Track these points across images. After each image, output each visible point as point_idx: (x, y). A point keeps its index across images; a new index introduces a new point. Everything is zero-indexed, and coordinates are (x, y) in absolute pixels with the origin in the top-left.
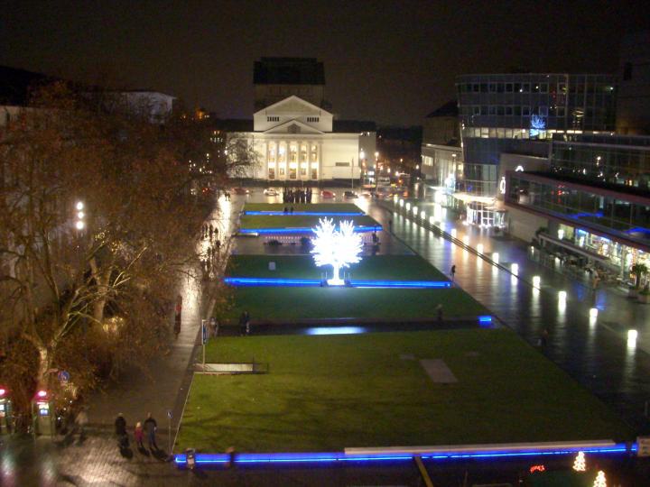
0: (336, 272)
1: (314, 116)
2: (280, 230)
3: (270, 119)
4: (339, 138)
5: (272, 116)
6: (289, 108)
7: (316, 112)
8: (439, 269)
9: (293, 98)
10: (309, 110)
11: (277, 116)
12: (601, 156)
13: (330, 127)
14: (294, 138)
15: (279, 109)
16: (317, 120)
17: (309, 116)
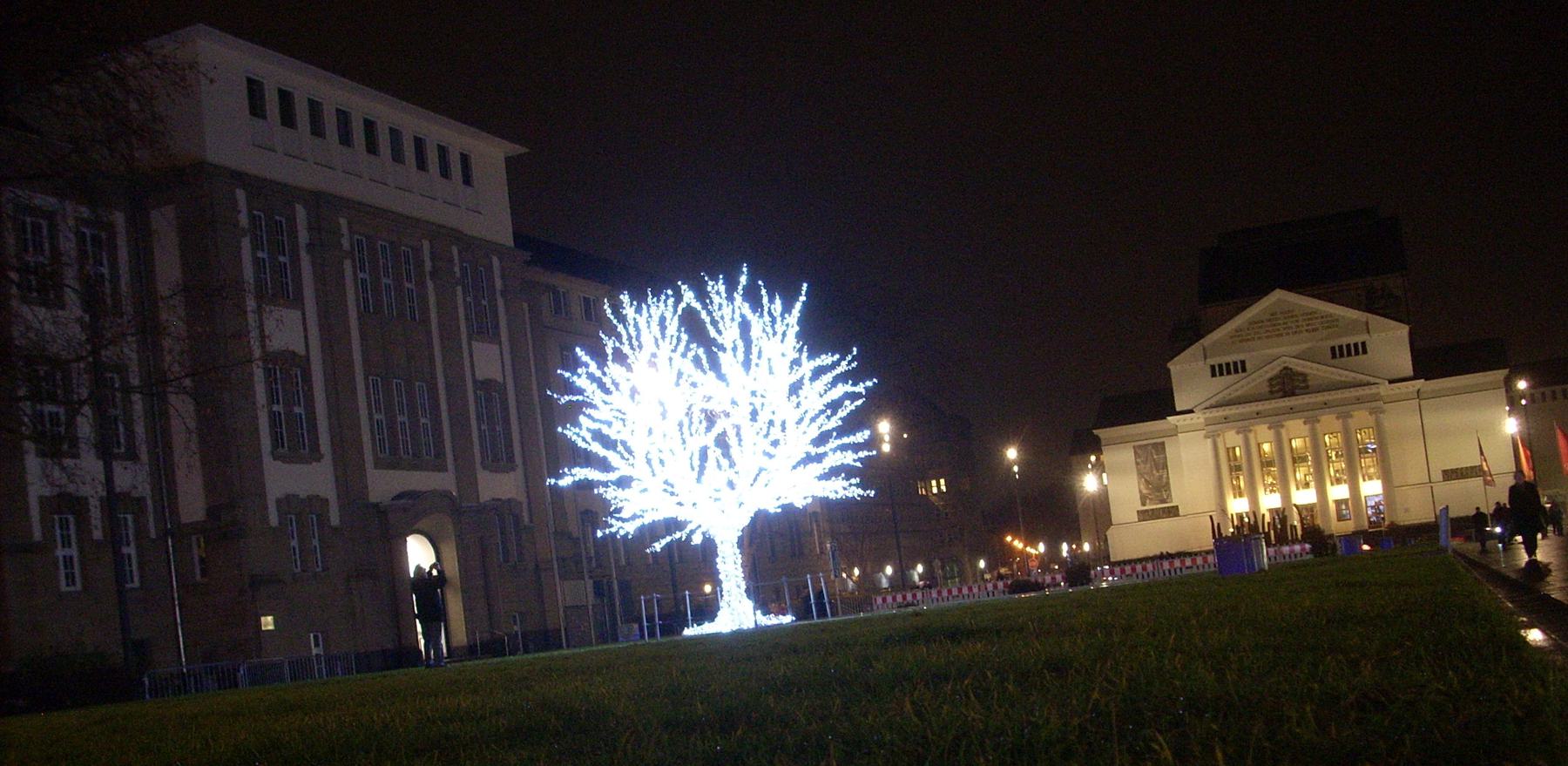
0: (731, 568)
1: (1352, 340)
2: (444, 415)
3: (1216, 371)
4: (1456, 392)
5: (1224, 360)
6: (1273, 326)
7: (1353, 327)
8: (454, 544)
9: (1278, 295)
10: (1331, 322)
11: (1237, 357)
12: (1007, 442)
13: (1405, 364)
14: (1292, 411)
15: (1240, 337)
16: (1362, 349)
17: (1336, 343)
